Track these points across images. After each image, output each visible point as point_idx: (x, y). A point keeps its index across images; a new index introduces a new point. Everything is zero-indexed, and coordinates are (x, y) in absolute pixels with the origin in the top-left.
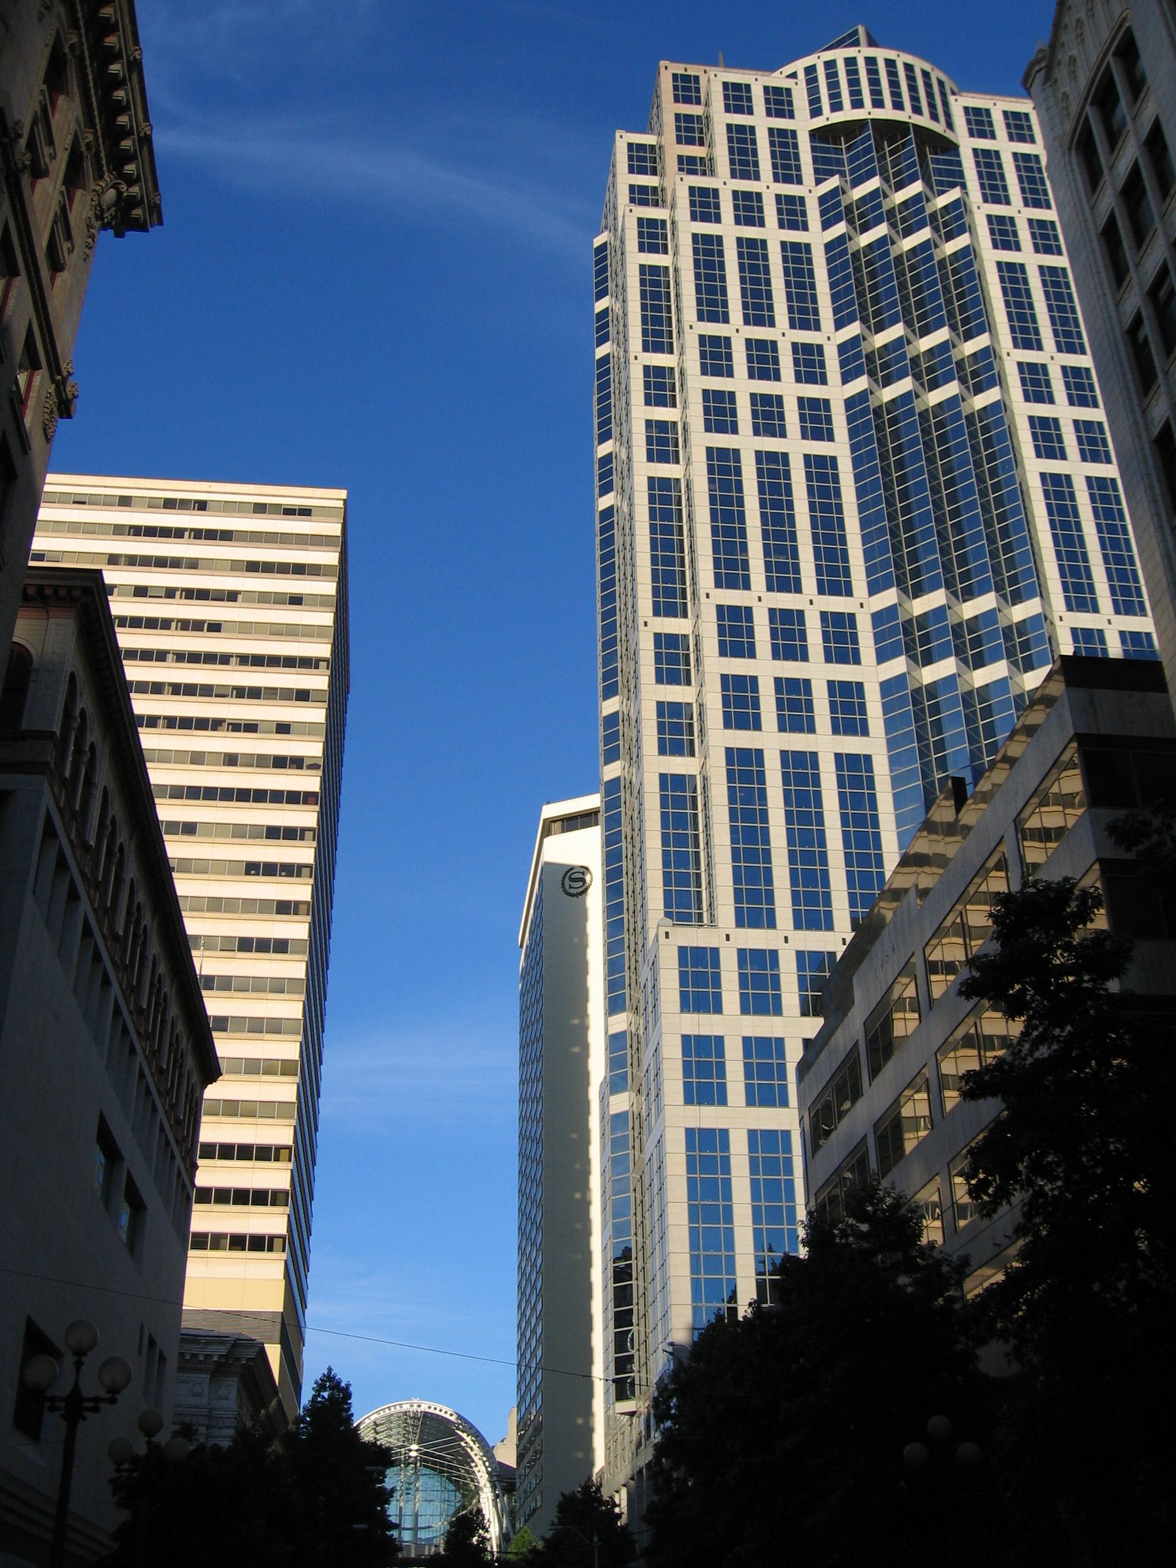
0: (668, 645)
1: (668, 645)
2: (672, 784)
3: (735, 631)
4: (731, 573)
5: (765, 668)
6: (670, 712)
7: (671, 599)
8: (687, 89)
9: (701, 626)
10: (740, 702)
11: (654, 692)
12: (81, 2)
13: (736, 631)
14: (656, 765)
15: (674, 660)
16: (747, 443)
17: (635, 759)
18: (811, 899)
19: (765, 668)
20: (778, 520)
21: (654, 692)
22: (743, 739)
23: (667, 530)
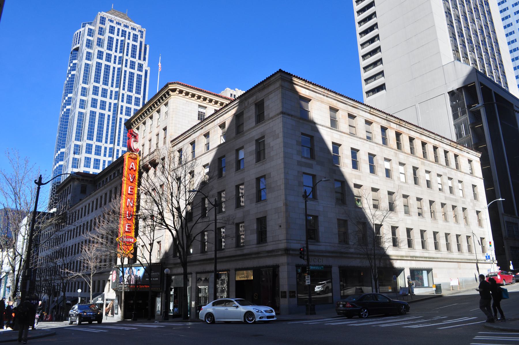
0: (84, 89)
1: (84, 89)
2: (80, 114)
3: (96, 90)
4: (97, 80)
5: (99, 98)
6: (82, 101)
7: (78, 138)
8: (103, 21)
9: (90, 86)
10: (94, 103)
11: (80, 97)
12: (466, 1)
13: (94, 103)
14: (78, 110)
15: (84, 92)
16: (104, 62)
17: (76, 95)
18: (99, 137)
19: (99, 98)
20: (107, 72)
21: (80, 97)
22: (95, 97)
23: (79, 130)
